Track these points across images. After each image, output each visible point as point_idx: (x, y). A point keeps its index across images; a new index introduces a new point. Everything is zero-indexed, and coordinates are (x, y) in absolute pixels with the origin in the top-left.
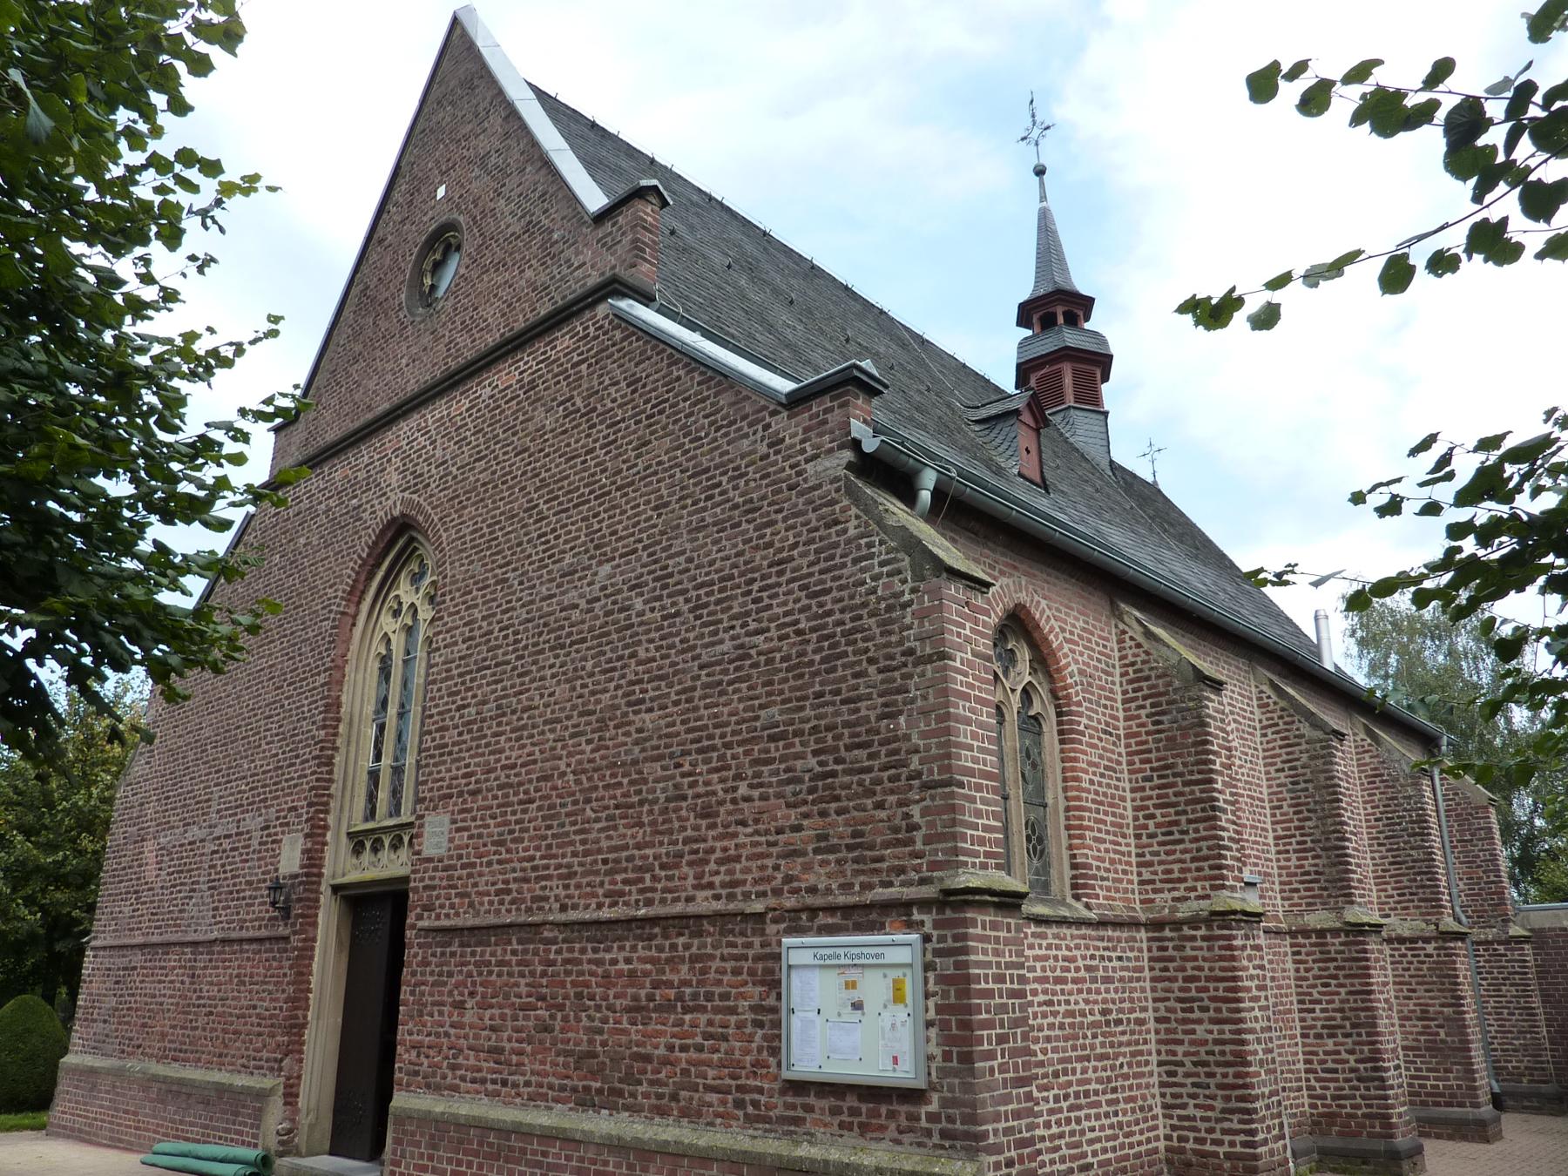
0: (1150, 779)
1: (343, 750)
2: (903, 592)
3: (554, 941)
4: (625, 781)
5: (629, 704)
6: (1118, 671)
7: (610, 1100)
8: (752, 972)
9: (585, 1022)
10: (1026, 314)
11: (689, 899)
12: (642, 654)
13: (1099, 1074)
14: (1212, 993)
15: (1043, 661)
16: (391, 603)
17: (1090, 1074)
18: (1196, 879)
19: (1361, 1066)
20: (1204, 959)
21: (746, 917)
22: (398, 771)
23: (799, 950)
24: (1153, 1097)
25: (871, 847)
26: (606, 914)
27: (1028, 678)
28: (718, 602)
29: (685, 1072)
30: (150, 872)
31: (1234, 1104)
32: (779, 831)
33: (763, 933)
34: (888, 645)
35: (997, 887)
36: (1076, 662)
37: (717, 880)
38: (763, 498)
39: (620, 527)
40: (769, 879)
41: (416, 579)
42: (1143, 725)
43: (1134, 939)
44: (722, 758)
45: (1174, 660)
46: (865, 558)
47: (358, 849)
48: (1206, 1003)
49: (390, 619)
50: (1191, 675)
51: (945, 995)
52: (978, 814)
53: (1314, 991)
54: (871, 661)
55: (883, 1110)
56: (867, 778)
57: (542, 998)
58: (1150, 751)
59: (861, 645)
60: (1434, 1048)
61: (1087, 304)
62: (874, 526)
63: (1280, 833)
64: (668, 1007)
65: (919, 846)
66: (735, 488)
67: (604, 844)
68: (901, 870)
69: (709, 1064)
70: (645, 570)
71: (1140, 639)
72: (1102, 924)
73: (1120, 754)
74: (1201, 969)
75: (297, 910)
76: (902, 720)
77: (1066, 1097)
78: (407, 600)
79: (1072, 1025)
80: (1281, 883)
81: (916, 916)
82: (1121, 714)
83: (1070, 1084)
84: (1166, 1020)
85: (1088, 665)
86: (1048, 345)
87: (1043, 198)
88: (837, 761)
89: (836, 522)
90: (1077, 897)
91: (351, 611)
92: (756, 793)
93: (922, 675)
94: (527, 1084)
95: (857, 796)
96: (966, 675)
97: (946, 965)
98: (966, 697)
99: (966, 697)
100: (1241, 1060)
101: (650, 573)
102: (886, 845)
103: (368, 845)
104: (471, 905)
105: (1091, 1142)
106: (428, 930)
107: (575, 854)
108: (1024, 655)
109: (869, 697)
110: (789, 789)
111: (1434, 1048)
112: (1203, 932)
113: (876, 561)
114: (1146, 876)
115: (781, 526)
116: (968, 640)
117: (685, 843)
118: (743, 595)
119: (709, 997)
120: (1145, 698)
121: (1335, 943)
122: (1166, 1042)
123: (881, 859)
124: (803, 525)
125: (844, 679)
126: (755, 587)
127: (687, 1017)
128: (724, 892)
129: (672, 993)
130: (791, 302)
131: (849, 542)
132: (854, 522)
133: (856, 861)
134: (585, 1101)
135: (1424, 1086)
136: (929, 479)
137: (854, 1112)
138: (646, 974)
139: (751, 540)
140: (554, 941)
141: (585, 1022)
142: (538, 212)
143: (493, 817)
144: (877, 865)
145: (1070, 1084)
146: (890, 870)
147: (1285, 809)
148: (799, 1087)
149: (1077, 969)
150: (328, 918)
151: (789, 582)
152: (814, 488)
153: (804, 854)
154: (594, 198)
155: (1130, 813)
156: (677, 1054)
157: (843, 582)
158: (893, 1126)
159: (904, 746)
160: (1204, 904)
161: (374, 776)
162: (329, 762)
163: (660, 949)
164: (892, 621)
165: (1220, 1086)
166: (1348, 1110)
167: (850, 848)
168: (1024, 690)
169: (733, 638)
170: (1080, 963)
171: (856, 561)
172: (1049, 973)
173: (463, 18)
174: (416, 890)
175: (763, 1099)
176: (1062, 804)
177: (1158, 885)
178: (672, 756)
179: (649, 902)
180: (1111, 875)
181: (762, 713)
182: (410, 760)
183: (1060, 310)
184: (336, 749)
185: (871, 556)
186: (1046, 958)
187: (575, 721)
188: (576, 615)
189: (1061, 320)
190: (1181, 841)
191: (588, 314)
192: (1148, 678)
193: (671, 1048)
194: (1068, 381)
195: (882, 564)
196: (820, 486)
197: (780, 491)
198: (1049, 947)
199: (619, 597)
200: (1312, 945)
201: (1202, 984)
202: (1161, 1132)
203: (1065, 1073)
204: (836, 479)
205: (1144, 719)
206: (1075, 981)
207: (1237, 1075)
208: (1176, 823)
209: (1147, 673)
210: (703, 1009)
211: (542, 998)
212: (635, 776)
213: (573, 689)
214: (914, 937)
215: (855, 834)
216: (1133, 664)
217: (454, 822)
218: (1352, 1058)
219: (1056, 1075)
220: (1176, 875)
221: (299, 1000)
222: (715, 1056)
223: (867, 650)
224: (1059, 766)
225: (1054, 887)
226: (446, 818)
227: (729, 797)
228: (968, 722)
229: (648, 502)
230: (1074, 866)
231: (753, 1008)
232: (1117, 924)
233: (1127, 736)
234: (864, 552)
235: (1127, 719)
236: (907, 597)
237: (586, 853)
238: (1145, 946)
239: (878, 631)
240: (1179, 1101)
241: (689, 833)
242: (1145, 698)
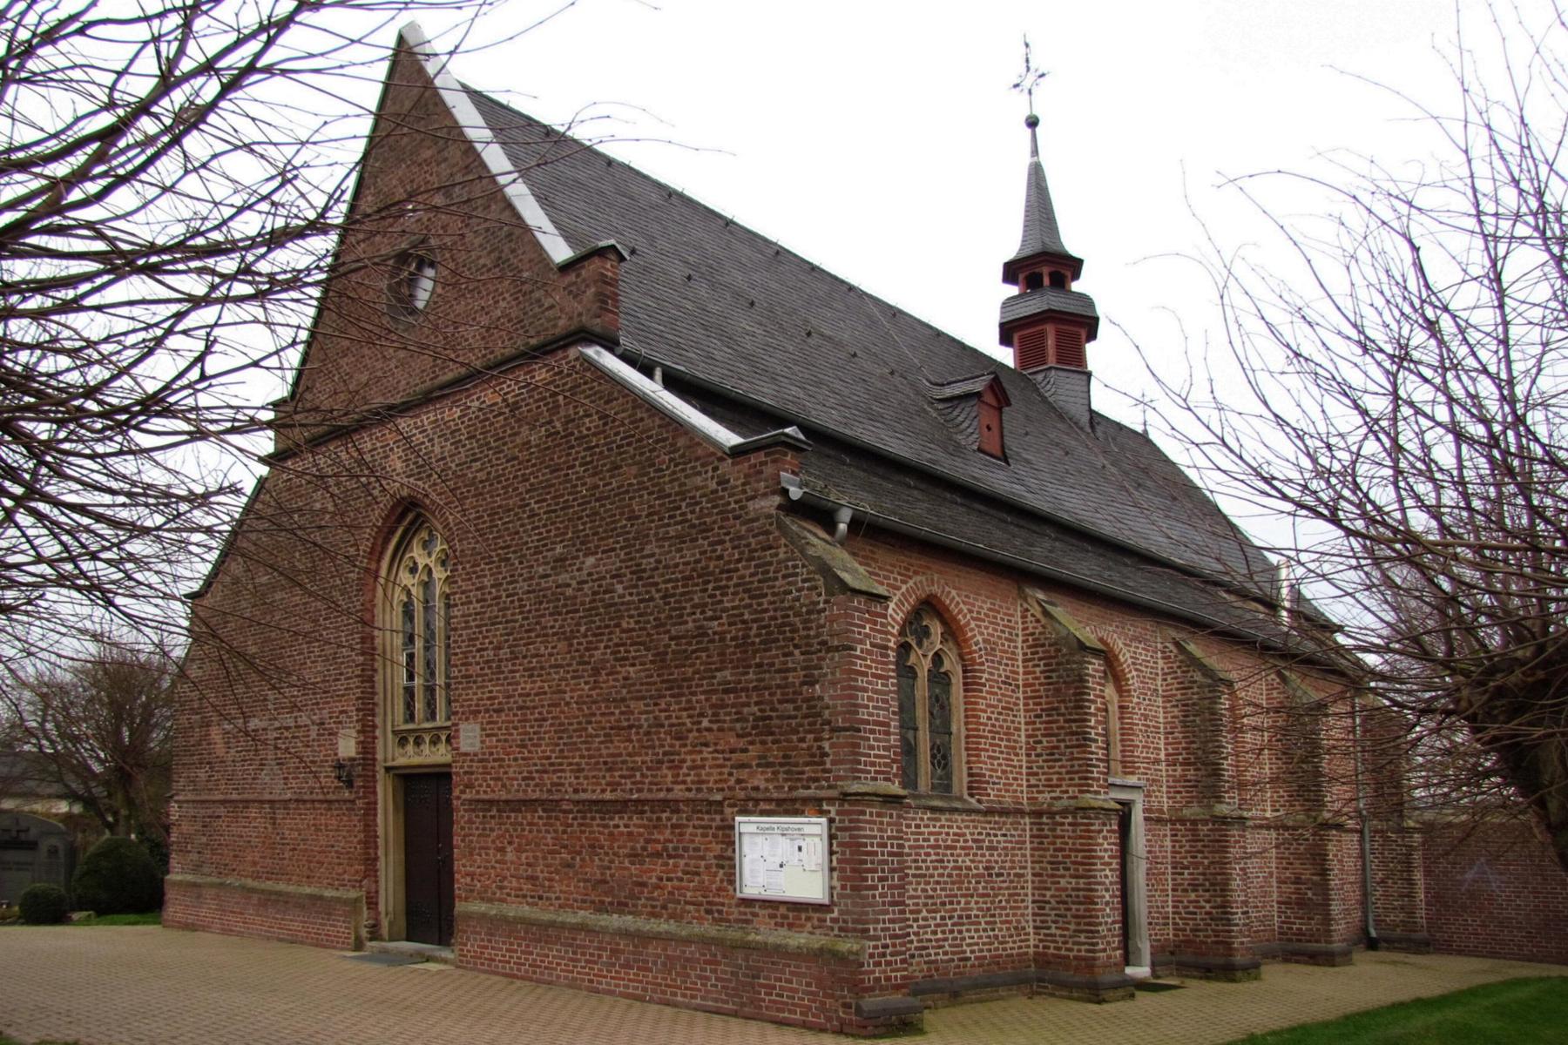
0: (1039, 716)
1: (381, 671)
3: (571, 811)
5: (616, 660)
6: (1020, 639)
7: (621, 907)
8: (714, 836)
9: (597, 861)
10: (1011, 272)
11: (669, 790)
12: (624, 625)
15: (953, 632)
16: (406, 561)
21: (710, 803)
22: (430, 690)
23: (746, 825)
25: (796, 765)
26: (608, 796)
27: (939, 646)
30: (220, 749)
31: (1083, 927)
32: (732, 751)
33: (722, 812)
34: (808, 636)
35: (881, 791)
37: (689, 779)
38: (715, 522)
40: (725, 781)
41: (426, 545)
44: (689, 701)
45: (1064, 633)
47: (403, 742)
49: (407, 575)
50: (1075, 645)
51: (843, 853)
52: (872, 748)
54: (796, 646)
55: (803, 916)
56: (794, 722)
57: (565, 847)
60: (1302, 903)
61: (1074, 266)
62: (797, 554)
64: (658, 855)
65: (828, 766)
66: (693, 512)
67: (604, 752)
68: (816, 780)
69: (688, 889)
71: (1039, 616)
72: (989, 812)
75: (359, 783)
78: (421, 562)
81: (825, 807)
82: (1021, 670)
84: (1040, 875)
86: (1035, 305)
87: (1035, 152)
89: (770, 548)
90: (972, 795)
91: (373, 566)
92: (715, 726)
93: (832, 659)
94: (558, 898)
95: (786, 733)
97: (844, 837)
98: (865, 674)
99: (865, 674)
100: (1091, 901)
102: (807, 764)
103: (411, 740)
104: (504, 786)
106: (471, 801)
107: (582, 757)
108: (936, 629)
109: (795, 670)
110: (738, 725)
111: (1302, 903)
112: (1070, 820)
114: (1033, 782)
115: (728, 545)
116: (867, 635)
119: (686, 849)
121: (1204, 829)
123: (803, 773)
125: (777, 656)
126: (710, 586)
130: (752, 304)
131: (779, 562)
134: (600, 908)
136: (845, 516)
137: (784, 917)
138: (640, 835)
140: (571, 811)
141: (597, 861)
142: (506, 250)
143: (515, 728)
148: (748, 902)
150: (384, 792)
152: (753, 520)
154: (560, 251)
155: (1023, 739)
159: (820, 704)
160: (1072, 802)
161: (409, 692)
162: (371, 680)
163: (650, 820)
164: (810, 621)
167: (781, 765)
168: (936, 654)
171: (784, 577)
173: (406, 35)
174: (457, 774)
176: (963, 733)
178: (651, 697)
181: (718, 674)
182: (440, 680)
183: (1045, 271)
184: (375, 671)
185: (796, 575)
187: (574, 667)
188: (569, 592)
189: (1046, 281)
191: (560, 354)
193: (661, 879)
194: (1051, 342)
195: (804, 581)
196: (757, 519)
198: (942, 826)
202: (1032, 943)
203: (951, 903)
204: (769, 516)
208: (1057, 748)
210: (682, 857)
211: (565, 847)
213: (571, 645)
214: (824, 820)
215: (785, 757)
217: (483, 729)
221: (370, 840)
224: (962, 707)
225: (955, 789)
226: (478, 727)
228: (865, 690)
230: (970, 775)
231: (715, 857)
232: (1004, 812)
237: (590, 757)
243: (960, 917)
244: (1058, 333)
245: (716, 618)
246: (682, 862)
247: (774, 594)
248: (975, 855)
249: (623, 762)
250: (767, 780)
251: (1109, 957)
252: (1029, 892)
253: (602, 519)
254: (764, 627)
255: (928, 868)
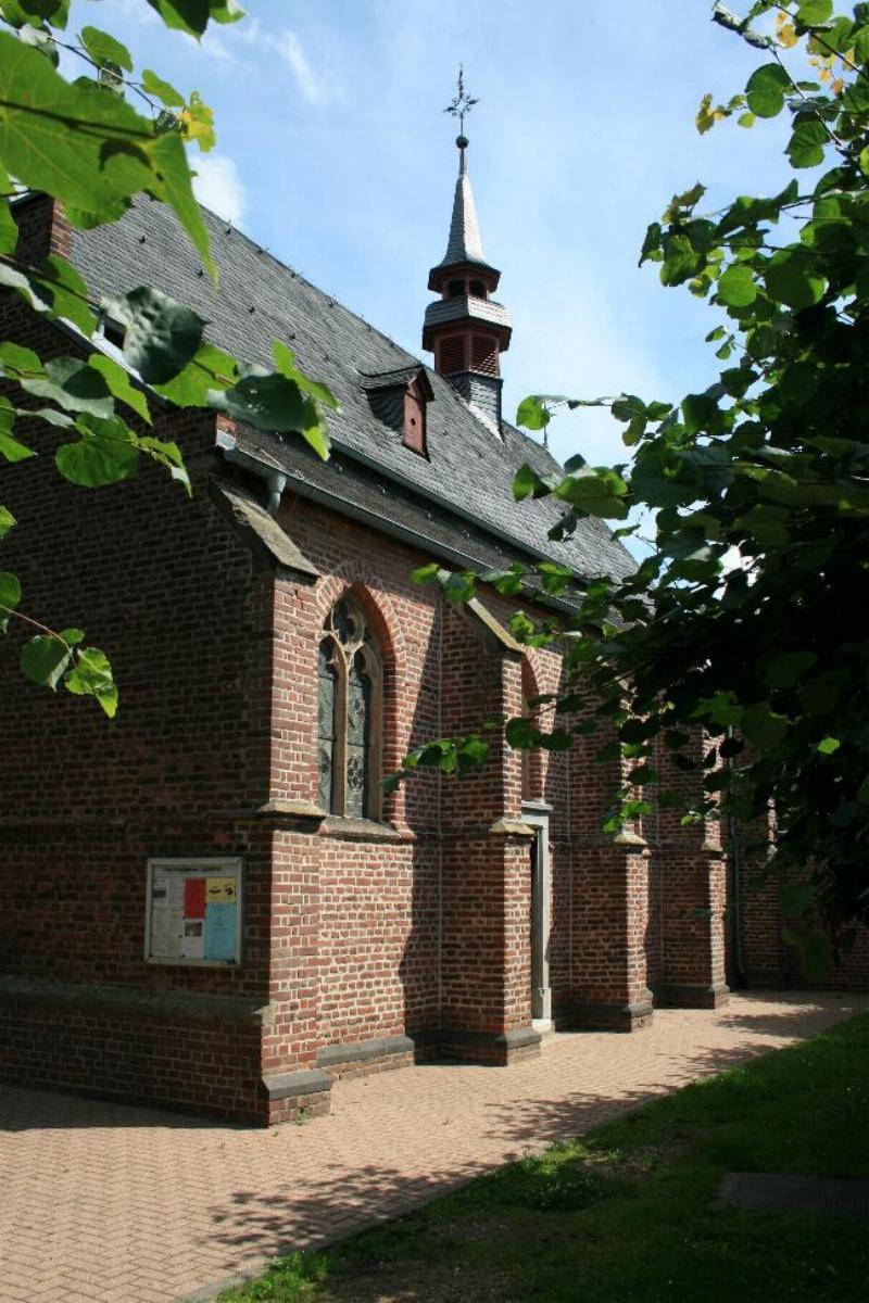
0: (456, 727)
2: (245, 581)
4: (17, 715)
13: (390, 952)
14: (486, 894)
17: (383, 952)
18: (484, 807)
19: (613, 951)
20: (483, 868)
24: (437, 970)
28: (100, 572)
29: (60, 945)
32: (139, 763)
36: (404, 630)
37: (89, 798)
39: (21, 497)
42: (457, 683)
43: (431, 852)
46: (220, 548)
48: (481, 901)
52: (288, 756)
53: (586, 895)
54: (217, 633)
58: (459, 705)
59: (211, 619)
62: (227, 524)
63: (576, 771)
65: (243, 779)
70: (41, 537)
73: (436, 706)
74: (479, 875)
76: (238, 681)
77: (361, 968)
79: (371, 916)
80: (572, 811)
82: (440, 673)
83: (365, 959)
85: (415, 633)
88: (188, 710)
89: (199, 516)
96: (288, 649)
101: (45, 540)
105: (378, 1001)
110: (148, 730)
113: (227, 552)
114: (447, 804)
115: (155, 513)
117: (64, 768)
118: (121, 567)
120: (460, 661)
122: (450, 930)
123: (213, 788)
124: (172, 514)
126: (131, 562)
127: (62, 903)
128: (94, 808)
129: (50, 884)
132: (212, 518)
133: (197, 788)
135: (676, 968)
139: (129, 522)
144: (210, 792)
145: (365, 959)
146: (220, 797)
147: (581, 752)
149: (379, 874)
151: (159, 561)
153: (156, 780)
156: (54, 931)
157: (200, 566)
158: (211, 982)
165: (484, 962)
166: (600, 983)
167: (193, 778)
169: (111, 604)
170: (382, 869)
171: (212, 550)
172: (354, 876)
175: (118, 964)
177: (456, 811)
179: (34, 814)
180: (419, 802)
185: (224, 548)
186: (353, 865)
190: (476, 778)
192: (463, 646)
197: (156, 483)
198: (356, 857)
199: (18, 558)
200: (588, 859)
201: (479, 887)
203: (361, 950)
205: (457, 679)
206: (375, 883)
207: (497, 954)
209: (463, 641)
210: (74, 897)
212: (25, 712)
216: (454, 633)
218: (607, 945)
219: (353, 952)
220: (469, 804)
222: (84, 932)
223: (214, 624)
227: (102, 732)
229: (46, 477)
233: (444, 692)
234: (219, 543)
235: (445, 677)
236: (248, 584)
238: (441, 857)
239: (223, 609)
240: (455, 973)
241: (68, 760)
242: (460, 661)
243: (370, 967)
244: (476, 339)
245: (136, 600)
246: (74, 904)
247: (198, 571)
248: (388, 891)
249: (20, 778)
250: (175, 798)
251: (518, 1009)
252: (440, 933)
253: (25, 484)
254: (185, 610)
255: (339, 908)
